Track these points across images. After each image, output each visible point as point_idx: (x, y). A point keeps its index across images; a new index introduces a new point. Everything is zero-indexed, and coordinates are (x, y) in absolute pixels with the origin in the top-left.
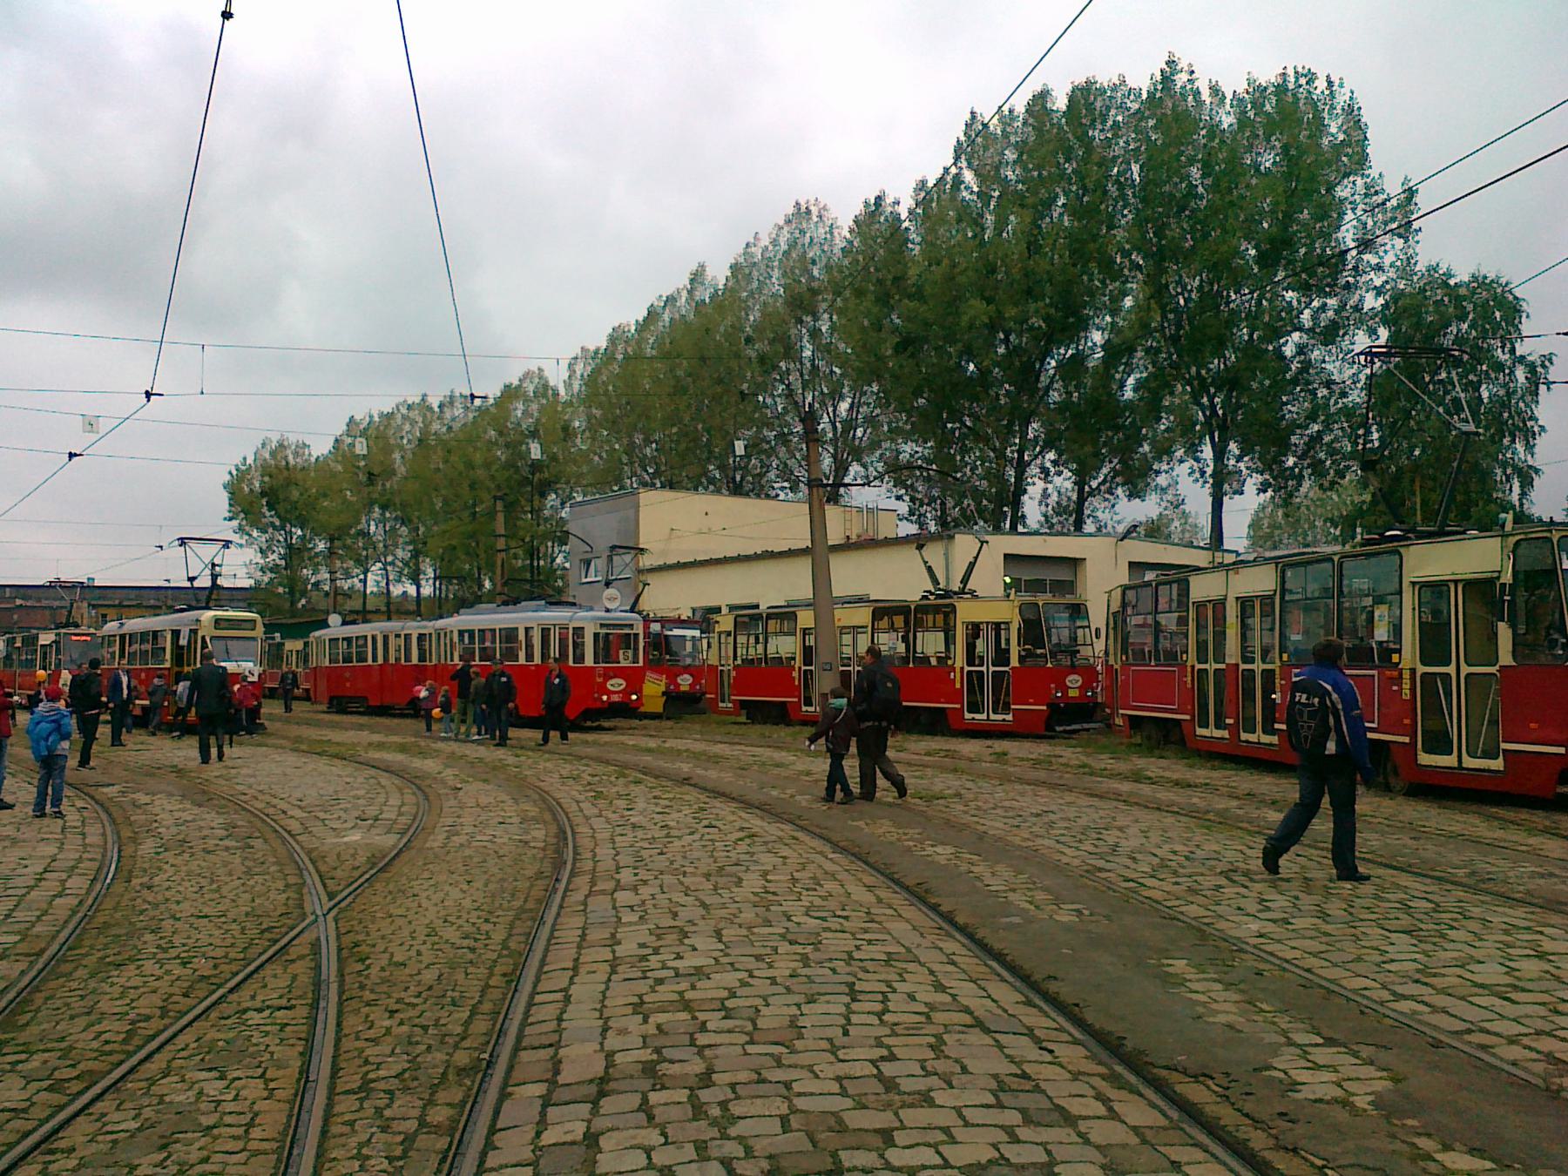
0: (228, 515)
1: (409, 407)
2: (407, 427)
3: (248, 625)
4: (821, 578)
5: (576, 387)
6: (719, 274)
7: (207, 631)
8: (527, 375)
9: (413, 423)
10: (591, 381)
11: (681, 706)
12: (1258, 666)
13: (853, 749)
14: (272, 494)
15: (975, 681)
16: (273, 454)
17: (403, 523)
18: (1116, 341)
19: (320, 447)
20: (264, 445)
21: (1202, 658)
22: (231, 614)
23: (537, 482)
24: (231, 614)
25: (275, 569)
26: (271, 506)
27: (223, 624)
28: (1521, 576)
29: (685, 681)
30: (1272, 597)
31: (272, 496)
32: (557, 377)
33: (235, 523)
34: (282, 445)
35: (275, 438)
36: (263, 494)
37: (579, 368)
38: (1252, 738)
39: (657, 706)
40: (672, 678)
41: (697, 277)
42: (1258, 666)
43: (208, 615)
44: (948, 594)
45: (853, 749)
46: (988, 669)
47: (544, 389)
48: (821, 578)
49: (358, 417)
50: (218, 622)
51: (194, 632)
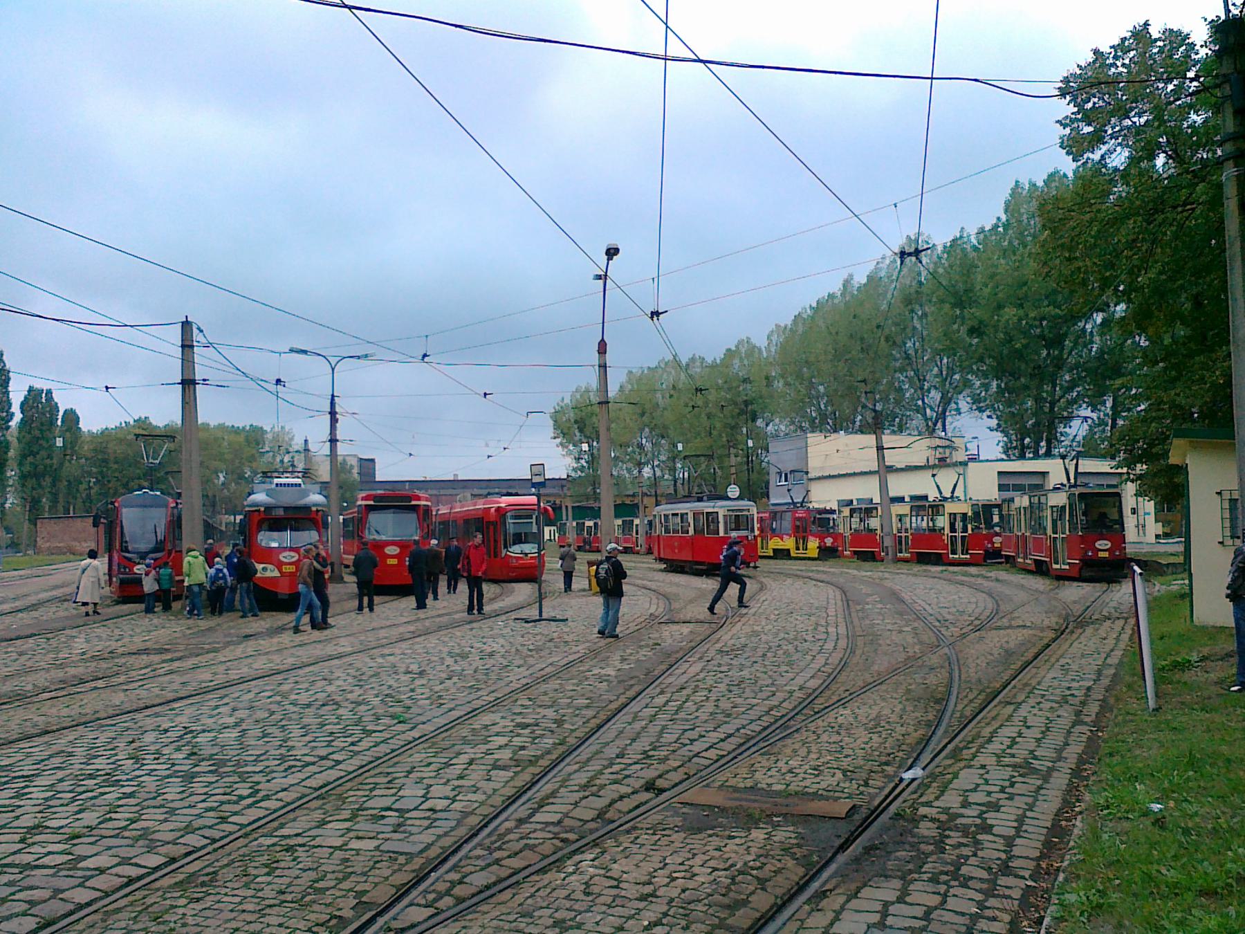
2: (665, 376)
4: (884, 487)
5: (773, 350)
6: (861, 278)
8: (740, 342)
10: (783, 348)
11: (827, 553)
12: (903, 535)
15: (953, 539)
17: (663, 437)
18: (764, 500)
21: (1055, 532)
23: (748, 411)
25: (582, 469)
26: (581, 431)
29: (829, 541)
30: (1063, 507)
31: (581, 424)
32: (761, 341)
33: (558, 440)
36: (576, 422)
37: (774, 338)
38: (1058, 566)
39: (815, 554)
40: (822, 539)
41: (847, 283)
42: (903, 535)
44: (945, 499)
46: (959, 534)
47: (753, 349)
48: (884, 487)
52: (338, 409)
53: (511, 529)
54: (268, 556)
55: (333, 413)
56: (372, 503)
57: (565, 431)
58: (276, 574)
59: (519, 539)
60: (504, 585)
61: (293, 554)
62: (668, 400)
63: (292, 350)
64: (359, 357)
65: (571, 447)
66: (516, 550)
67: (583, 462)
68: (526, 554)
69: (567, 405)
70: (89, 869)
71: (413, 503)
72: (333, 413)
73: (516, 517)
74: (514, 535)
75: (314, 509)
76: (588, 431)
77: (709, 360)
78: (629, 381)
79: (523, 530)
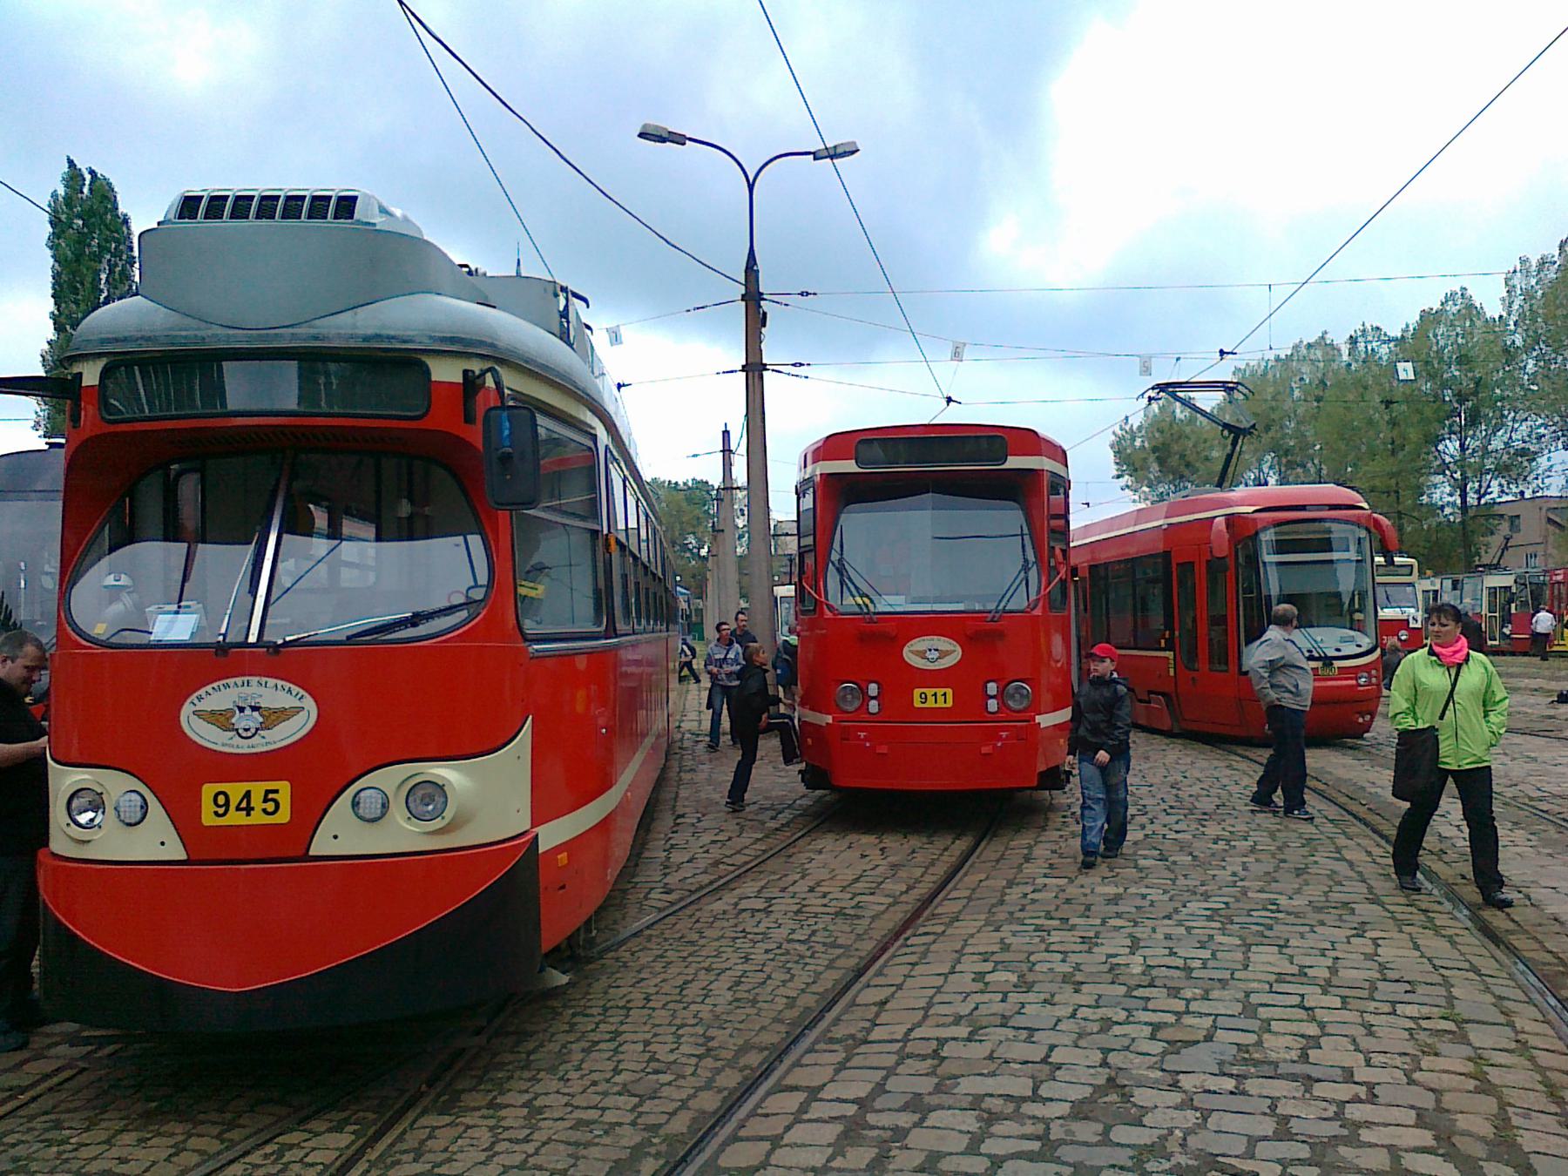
1: (1309, 346)
3: (1407, 571)
36: (1155, 450)
56: (850, 466)
58: (156, 841)
61: (273, 693)
68: (1328, 661)
71: (1013, 462)
73: (1281, 547)
75: (446, 372)
76: (1174, 461)
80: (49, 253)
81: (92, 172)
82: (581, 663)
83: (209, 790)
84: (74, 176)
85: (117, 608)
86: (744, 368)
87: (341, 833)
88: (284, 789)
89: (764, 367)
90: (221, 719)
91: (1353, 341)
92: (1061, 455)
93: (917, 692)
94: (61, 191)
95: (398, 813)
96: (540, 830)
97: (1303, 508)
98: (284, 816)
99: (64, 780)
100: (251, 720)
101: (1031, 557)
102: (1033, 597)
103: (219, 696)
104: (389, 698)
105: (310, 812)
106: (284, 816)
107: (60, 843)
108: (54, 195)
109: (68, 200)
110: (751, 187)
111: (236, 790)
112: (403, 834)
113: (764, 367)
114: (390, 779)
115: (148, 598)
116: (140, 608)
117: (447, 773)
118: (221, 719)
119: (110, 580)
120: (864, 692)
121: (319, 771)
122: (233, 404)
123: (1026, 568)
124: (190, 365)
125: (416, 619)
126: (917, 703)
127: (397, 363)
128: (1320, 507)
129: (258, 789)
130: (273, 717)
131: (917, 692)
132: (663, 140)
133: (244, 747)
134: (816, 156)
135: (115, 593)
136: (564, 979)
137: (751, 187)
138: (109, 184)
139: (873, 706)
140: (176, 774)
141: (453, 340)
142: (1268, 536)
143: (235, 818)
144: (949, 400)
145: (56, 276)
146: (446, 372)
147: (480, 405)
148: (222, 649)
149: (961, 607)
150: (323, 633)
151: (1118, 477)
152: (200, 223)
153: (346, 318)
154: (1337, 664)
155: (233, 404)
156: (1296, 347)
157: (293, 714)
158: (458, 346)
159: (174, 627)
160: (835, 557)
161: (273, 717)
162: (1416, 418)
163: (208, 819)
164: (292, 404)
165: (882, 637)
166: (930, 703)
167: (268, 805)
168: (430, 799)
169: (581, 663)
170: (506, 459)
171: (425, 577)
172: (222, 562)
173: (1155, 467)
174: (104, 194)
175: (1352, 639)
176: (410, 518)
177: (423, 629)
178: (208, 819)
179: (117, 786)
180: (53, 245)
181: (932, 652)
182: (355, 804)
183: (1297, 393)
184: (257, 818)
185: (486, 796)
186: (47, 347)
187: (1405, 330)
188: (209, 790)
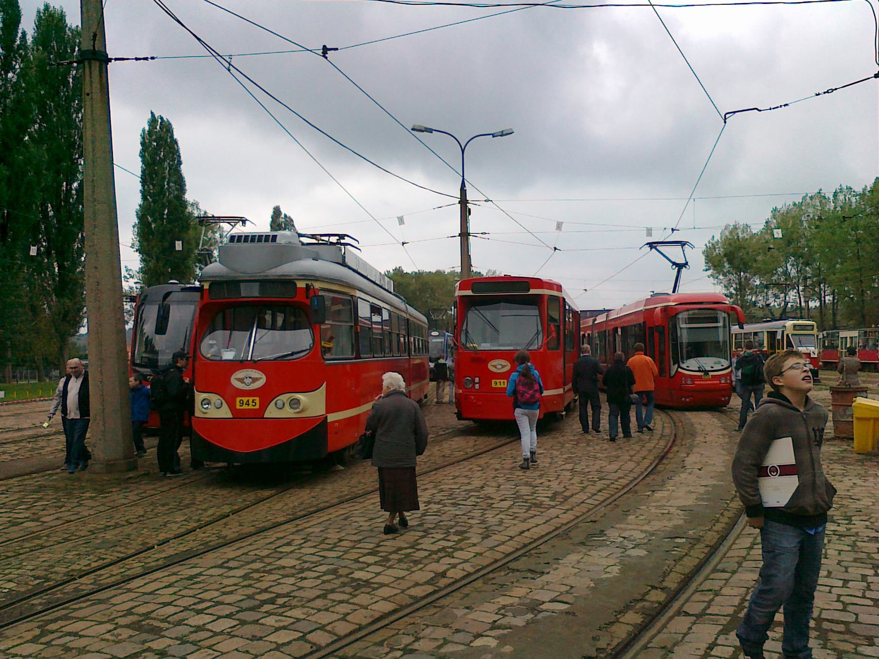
0: (705, 268)
1: (811, 198)
3: (810, 328)
7: (789, 331)
9: (814, 206)
13: (781, 610)
14: (733, 255)
16: (731, 233)
19: (757, 227)
20: (725, 229)
22: (801, 322)
24: (801, 322)
25: (730, 296)
27: (797, 328)
28: (605, 388)
33: (710, 272)
34: (735, 228)
35: (732, 224)
36: (725, 255)
43: (789, 323)
45: (781, 610)
49: (779, 207)
50: (795, 326)
51: (783, 332)
52: (469, 197)
53: (684, 337)
54: (218, 377)
55: (464, 202)
56: (469, 293)
57: (716, 263)
58: (225, 413)
59: (698, 350)
60: (677, 415)
61: (255, 373)
62: (814, 230)
63: (337, 49)
64: (494, 136)
65: (721, 277)
66: (692, 365)
67: (732, 290)
68: (706, 372)
69: (717, 242)
70: (355, 604)
71: (533, 291)
72: (464, 202)
73: (691, 320)
74: (689, 344)
75: (301, 285)
76: (737, 262)
77: (859, 189)
78: (774, 217)
79: (702, 338)
80: (140, 159)
81: (162, 118)
82: (348, 368)
83: (238, 399)
84: (153, 121)
85: (212, 350)
86: (460, 235)
87: (272, 412)
88: (257, 400)
89: (469, 234)
90: (241, 380)
91: (835, 195)
92: (559, 288)
93: (493, 381)
94: (147, 128)
95: (287, 406)
96: (329, 415)
97: (701, 303)
98: (257, 407)
99: (199, 397)
100: (248, 381)
101: (540, 328)
102: (540, 344)
103: (240, 374)
104: (285, 375)
105: (264, 406)
106: (257, 407)
107: (198, 414)
108: (144, 130)
109: (150, 132)
110: (463, 151)
111: (245, 399)
112: (288, 413)
113: (469, 234)
114: (285, 398)
115: (219, 347)
116: (219, 350)
117: (299, 396)
118: (241, 380)
119: (211, 342)
120: (474, 381)
121: (266, 395)
122: (243, 295)
123: (538, 333)
124: (230, 284)
125: (292, 354)
126: (493, 385)
127: (287, 283)
128: (709, 303)
129: (251, 399)
130: (255, 380)
131: (493, 381)
132: (423, 131)
133: (247, 388)
134: (494, 136)
135: (211, 346)
136: (342, 468)
137: (463, 151)
138: (170, 124)
139: (477, 386)
140: (230, 395)
141: (302, 275)
142: (683, 316)
143: (245, 407)
144: (555, 249)
145: (143, 172)
146: (301, 285)
147: (311, 294)
148: (241, 361)
149: (511, 348)
150: (268, 357)
151: (707, 270)
152: (235, 245)
153: (273, 270)
154: (711, 373)
155: (243, 295)
156: (804, 198)
157: (259, 379)
158: (304, 277)
159: (228, 355)
160: (464, 328)
161: (255, 380)
162: (869, 239)
163: (238, 407)
164: (257, 294)
165: (482, 359)
166: (498, 386)
167: (253, 404)
168: (296, 404)
169: (348, 368)
170: (316, 311)
171: (301, 340)
172: (239, 336)
173: (727, 265)
174: (167, 128)
175: (719, 363)
176: (295, 322)
177: (295, 356)
178: (238, 407)
179: (215, 398)
180: (142, 155)
181: (498, 366)
182: (276, 404)
183: (805, 224)
184: (250, 407)
185: (313, 403)
186: (138, 207)
187: (864, 190)
188: (238, 399)
